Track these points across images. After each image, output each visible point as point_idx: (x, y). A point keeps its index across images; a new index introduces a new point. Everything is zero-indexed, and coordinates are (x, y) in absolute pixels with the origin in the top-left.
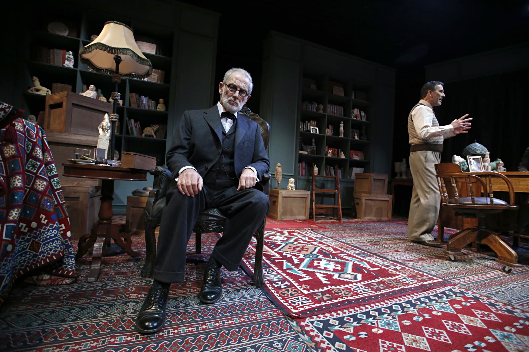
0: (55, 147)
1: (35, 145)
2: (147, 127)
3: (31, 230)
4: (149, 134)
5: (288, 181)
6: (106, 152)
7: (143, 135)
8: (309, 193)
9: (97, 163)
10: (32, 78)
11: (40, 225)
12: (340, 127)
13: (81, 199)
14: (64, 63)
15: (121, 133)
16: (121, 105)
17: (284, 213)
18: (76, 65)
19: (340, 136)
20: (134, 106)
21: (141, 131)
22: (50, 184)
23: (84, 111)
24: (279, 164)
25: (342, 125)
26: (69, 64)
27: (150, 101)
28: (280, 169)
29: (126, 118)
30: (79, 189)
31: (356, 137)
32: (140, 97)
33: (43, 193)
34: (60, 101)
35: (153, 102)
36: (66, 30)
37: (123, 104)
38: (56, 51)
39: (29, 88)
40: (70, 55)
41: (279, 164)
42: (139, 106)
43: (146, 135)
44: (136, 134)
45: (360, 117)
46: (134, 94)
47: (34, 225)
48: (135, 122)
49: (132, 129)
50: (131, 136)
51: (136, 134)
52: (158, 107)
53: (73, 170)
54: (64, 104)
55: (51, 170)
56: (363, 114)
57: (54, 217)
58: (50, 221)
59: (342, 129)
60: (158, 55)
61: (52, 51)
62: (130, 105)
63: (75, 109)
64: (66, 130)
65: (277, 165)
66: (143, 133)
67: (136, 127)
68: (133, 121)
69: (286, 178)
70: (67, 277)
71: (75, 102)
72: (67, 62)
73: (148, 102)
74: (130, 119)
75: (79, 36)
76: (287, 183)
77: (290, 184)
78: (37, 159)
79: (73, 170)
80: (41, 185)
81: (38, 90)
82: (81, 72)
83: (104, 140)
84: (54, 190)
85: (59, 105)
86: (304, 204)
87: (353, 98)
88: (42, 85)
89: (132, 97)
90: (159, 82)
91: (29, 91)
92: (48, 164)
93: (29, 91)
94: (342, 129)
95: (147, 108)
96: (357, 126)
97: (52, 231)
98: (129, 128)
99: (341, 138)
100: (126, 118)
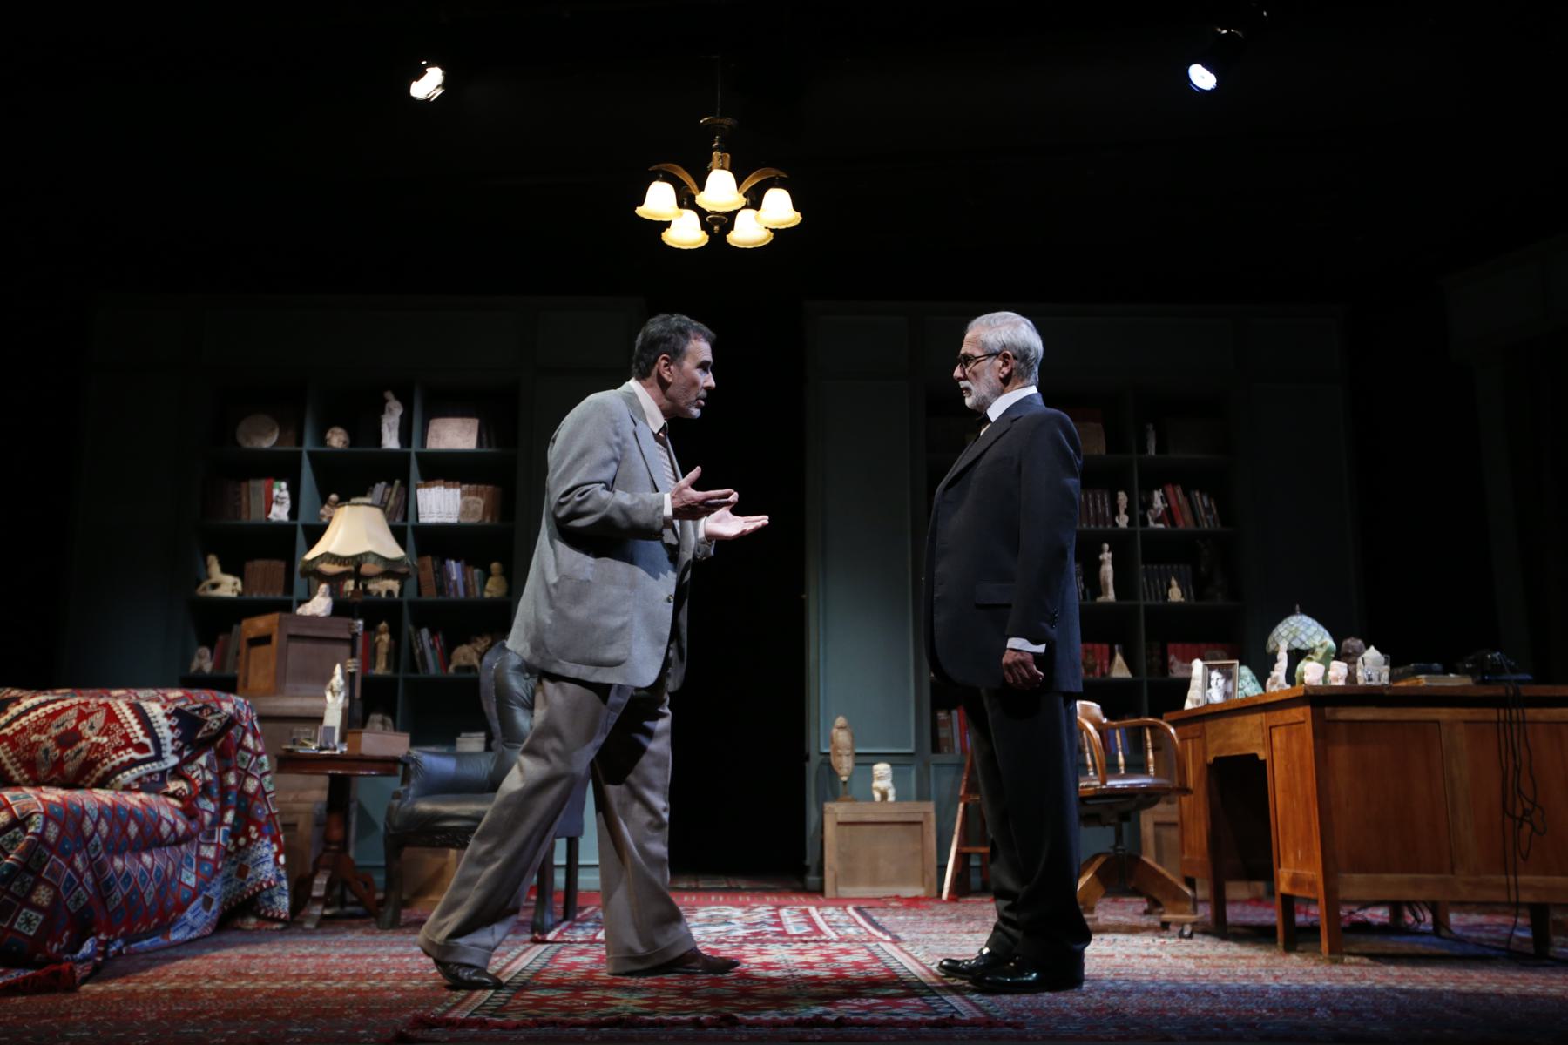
0: (270, 726)
1: (245, 730)
2: (460, 644)
3: (239, 848)
4: (464, 663)
5: (871, 772)
6: (337, 732)
7: (451, 669)
8: (930, 807)
9: (321, 749)
10: (205, 561)
11: (250, 841)
12: (1100, 563)
13: (300, 827)
14: (269, 511)
15: (396, 670)
16: (396, 595)
17: (850, 876)
18: (293, 513)
19: (1100, 599)
20: (430, 595)
21: (446, 659)
22: (261, 785)
23: (308, 646)
24: (840, 721)
25: (1107, 556)
26: (280, 513)
27: (469, 570)
28: (842, 737)
29: (408, 627)
30: (297, 806)
31: (1175, 594)
32: (443, 562)
33: (254, 796)
34: (266, 633)
35: (477, 571)
36: (272, 430)
37: (401, 592)
38: (259, 485)
39: (199, 583)
40: (281, 490)
41: (840, 721)
42: (441, 589)
43: (458, 669)
44: (433, 669)
45: (1188, 517)
46: (428, 560)
47: (242, 841)
48: (433, 633)
49: (423, 654)
50: (421, 674)
51: (433, 669)
52: (488, 586)
53: (289, 762)
54: (275, 638)
55: (262, 765)
56: (1203, 501)
57: (266, 829)
58: (262, 835)
59: (1107, 570)
60: (484, 450)
61: (244, 485)
62: (419, 594)
63: (295, 647)
64: (277, 690)
65: (833, 723)
66: (449, 662)
67: (433, 647)
68: (425, 633)
69: (865, 761)
70: (278, 920)
71: (292, 632)
72: (275, 508)
73: (464, 574)
74: (418, 627)
75: (300, 442)
76: (870, 778)
77: (876, 784)
78: (247, 750)
79: (289, 762)
80: (251, 785)
81: (215, 586)
82: (311, 455)
83: (334, 707)
84: (265, 794)
85: (265, 640)
86: (919, 847)
87: (1152, 451)
88: (225, 570)
89: (424, 567)
90: (488, 520)
91: (200, 592)
92: (259, 755)
93: (200, 592)
94: (1107, 570)
95: (462, 594)
96: (1167, 551)
97: (266, 850)
98: (417, 651)
99: (1108, 605)
100: (408, 627)
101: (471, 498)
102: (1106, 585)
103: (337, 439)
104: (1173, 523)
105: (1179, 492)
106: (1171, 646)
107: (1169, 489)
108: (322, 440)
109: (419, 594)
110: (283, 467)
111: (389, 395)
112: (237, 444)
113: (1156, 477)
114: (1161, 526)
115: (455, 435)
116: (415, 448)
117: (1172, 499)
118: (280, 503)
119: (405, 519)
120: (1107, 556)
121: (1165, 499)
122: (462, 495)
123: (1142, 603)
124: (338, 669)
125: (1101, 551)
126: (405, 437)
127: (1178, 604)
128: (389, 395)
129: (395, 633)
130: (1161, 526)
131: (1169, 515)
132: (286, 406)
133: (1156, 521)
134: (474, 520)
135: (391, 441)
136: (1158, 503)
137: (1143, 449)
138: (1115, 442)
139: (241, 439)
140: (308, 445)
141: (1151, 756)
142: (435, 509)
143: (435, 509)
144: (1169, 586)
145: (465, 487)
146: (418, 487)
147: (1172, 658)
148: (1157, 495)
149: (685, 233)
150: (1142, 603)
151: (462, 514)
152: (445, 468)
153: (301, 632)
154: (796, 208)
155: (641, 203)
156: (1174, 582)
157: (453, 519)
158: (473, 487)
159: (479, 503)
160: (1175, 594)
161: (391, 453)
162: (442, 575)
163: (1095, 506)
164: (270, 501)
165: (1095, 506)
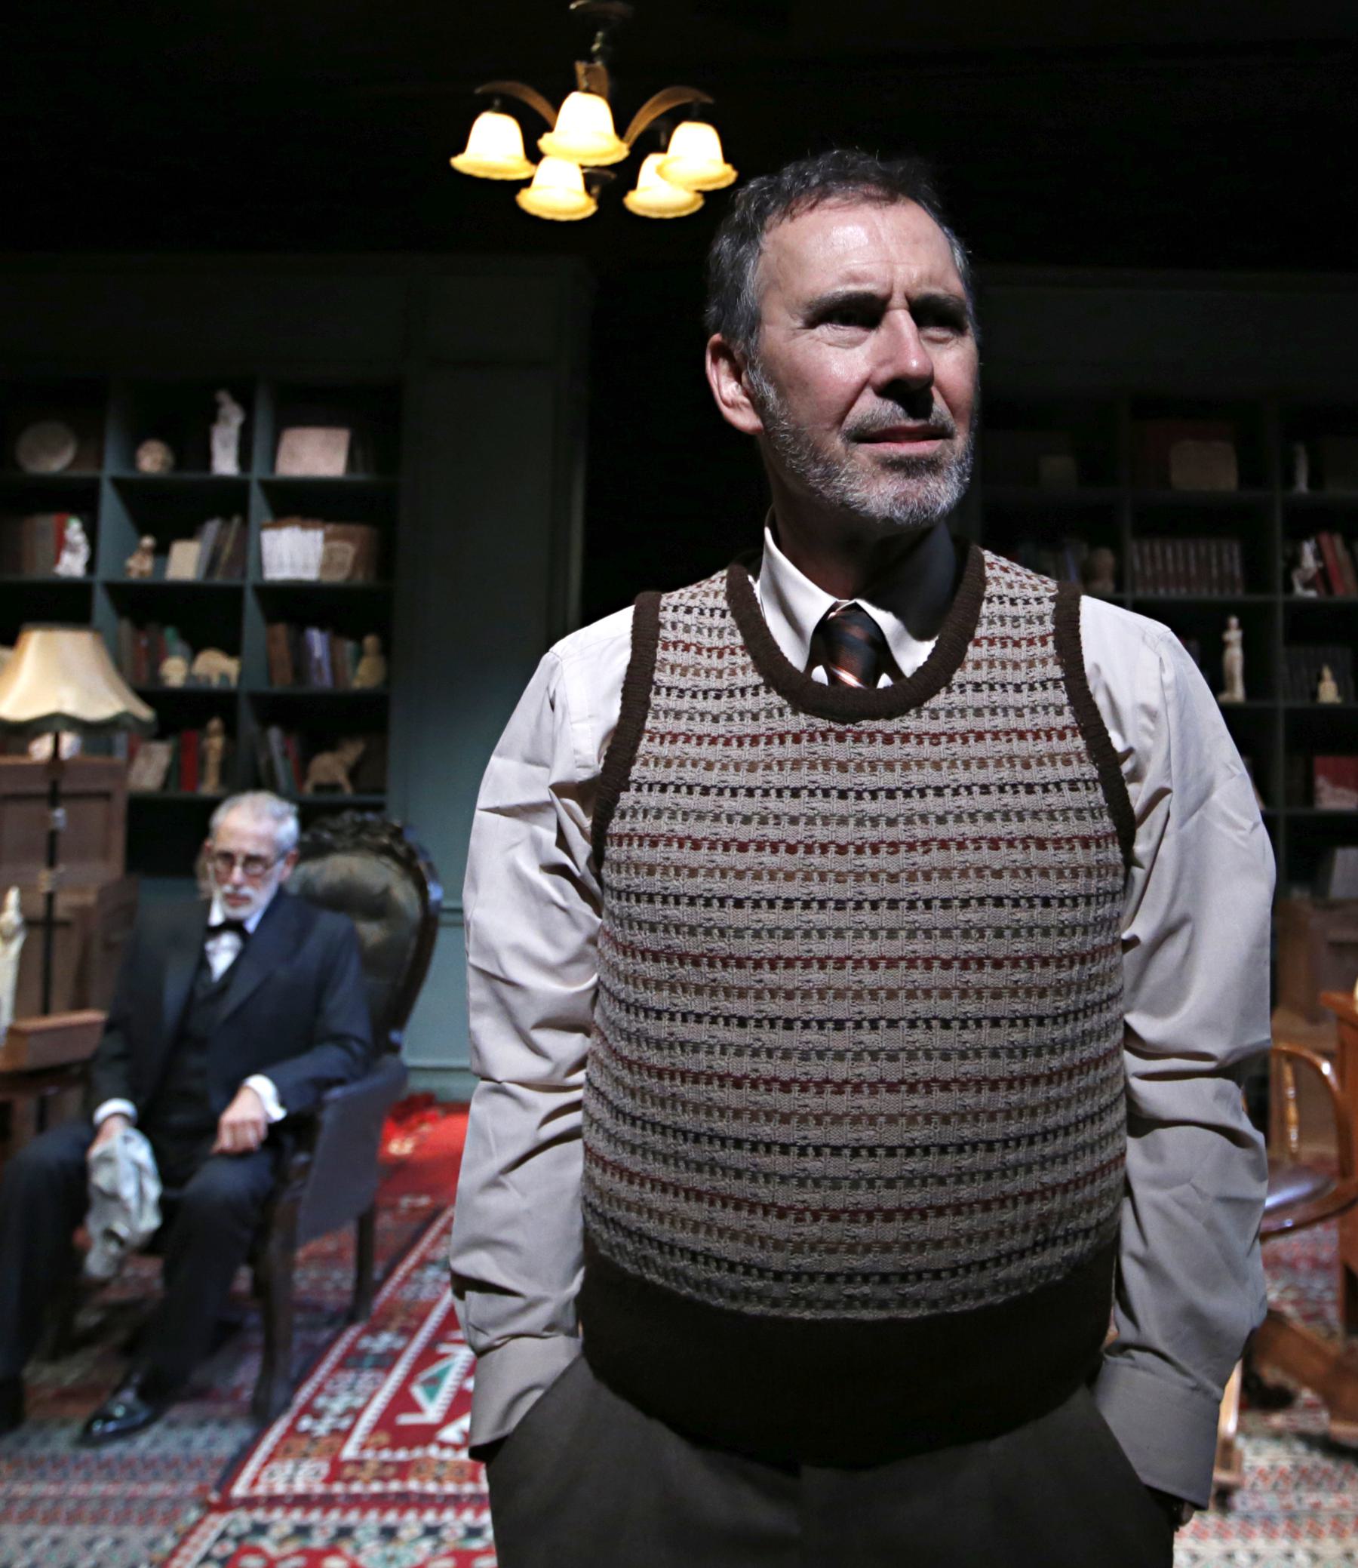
4: (324, 779)
14: (57, 559)
18: (91, 565)
25: (1234, 635)
26: (72, 564)
31: (1329, 692)
38: (46, 522)
40: (74, 530)
43: (319, 788)
49: (270, 764)
67: (285, 754)
73: (332, 649)
75: (100, 465)
82: (118, 483)
87: (1302, 486)
101: (336, 544)
102: (1232, 678)
103: (152, 459)
104: (1329, 590)
105: (1338, 542)
106: (1319, 761)
107: (1325, 539)
108: (132, 461)
109: (270, 681)
110: (76, 498)
111: (223, 397)
112: (17, 466)
113: (1306, 522)
114: (1312, 594)
115: (317, 455)
116: (258, 472)
117: (1329, 555)
118: (74, 550)
119: (244, 574)
120: (1234, 635)
121: (1319, 555)
122: (327, 538)
123: (1282, 703)
124: (13, 897)
125: (1225, 627)
126: (244, 458)
127: (1330, 710)
128: (223, 397)
129: (230, 731)
130: (1312, 594)
131: (1323, 579)
132: (80, 407)
133: (1307, 585)
134: (338, 577)
135: (225, 463)
136: (1309, 561)
137: (1290, 480)
138: (1250, 476)
139: (22, 457)
140: (112, 467)
141: (1292, 1113)
142: (286, 560)
143: (286, 560)
144: (1320, 678)
145: (330, 528)
146: (264, 527)
147: (1321, 782)
148: (1308, 549)
149: (557, 193)
150: (1280, 598)
151: (325, 567)
152: (300, 502)
153: (21, 789)
154: (728, 158)
155: (461, 147)
156: (1327, 673)
157: (311, 575)
158: (340, 528)
159: (347, 551)
160: (1329, 692)
161: (225, 481)
162: (300, 650)
163: (1220, 563)
164: (61, 544)
165: (1220, 563)
